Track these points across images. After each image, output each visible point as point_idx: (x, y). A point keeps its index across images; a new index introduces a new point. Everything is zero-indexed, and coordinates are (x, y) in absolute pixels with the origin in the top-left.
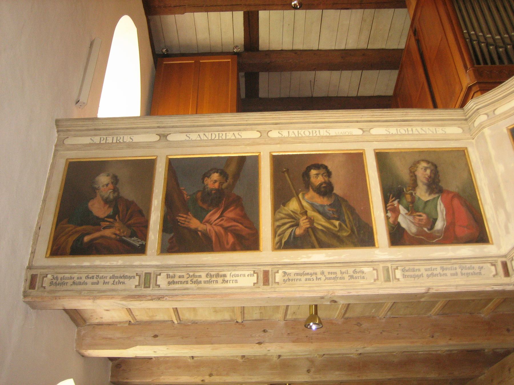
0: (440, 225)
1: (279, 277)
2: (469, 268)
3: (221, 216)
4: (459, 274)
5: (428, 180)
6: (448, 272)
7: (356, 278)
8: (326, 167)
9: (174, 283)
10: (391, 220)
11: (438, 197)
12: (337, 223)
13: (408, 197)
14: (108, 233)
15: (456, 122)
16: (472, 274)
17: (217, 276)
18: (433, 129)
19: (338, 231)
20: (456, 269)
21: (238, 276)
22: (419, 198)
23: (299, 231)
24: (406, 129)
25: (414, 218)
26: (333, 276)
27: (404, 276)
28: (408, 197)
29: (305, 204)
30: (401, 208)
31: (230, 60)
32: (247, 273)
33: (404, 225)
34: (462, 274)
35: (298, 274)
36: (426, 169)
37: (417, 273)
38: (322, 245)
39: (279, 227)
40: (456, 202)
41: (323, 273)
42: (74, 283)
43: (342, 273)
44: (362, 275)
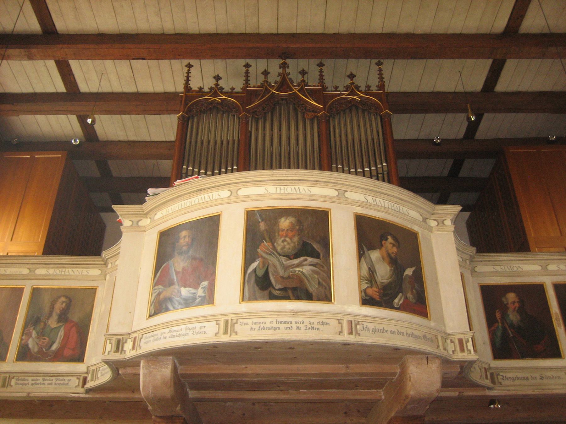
0: (55, 347)
2: (62, 380)
4: (54, 383)
6: (46, 382)
11: (60, 327)
13: (42, 324)
15: (97, 266)
16: (62, 385)
18: (80, 270)
20: (52, 380)
22: (49, 326)
24: (61, 270)
27: (16, 384)
33: (30, 346)
36: (63, 302)
37: (26, 382)
40: (74, 329)
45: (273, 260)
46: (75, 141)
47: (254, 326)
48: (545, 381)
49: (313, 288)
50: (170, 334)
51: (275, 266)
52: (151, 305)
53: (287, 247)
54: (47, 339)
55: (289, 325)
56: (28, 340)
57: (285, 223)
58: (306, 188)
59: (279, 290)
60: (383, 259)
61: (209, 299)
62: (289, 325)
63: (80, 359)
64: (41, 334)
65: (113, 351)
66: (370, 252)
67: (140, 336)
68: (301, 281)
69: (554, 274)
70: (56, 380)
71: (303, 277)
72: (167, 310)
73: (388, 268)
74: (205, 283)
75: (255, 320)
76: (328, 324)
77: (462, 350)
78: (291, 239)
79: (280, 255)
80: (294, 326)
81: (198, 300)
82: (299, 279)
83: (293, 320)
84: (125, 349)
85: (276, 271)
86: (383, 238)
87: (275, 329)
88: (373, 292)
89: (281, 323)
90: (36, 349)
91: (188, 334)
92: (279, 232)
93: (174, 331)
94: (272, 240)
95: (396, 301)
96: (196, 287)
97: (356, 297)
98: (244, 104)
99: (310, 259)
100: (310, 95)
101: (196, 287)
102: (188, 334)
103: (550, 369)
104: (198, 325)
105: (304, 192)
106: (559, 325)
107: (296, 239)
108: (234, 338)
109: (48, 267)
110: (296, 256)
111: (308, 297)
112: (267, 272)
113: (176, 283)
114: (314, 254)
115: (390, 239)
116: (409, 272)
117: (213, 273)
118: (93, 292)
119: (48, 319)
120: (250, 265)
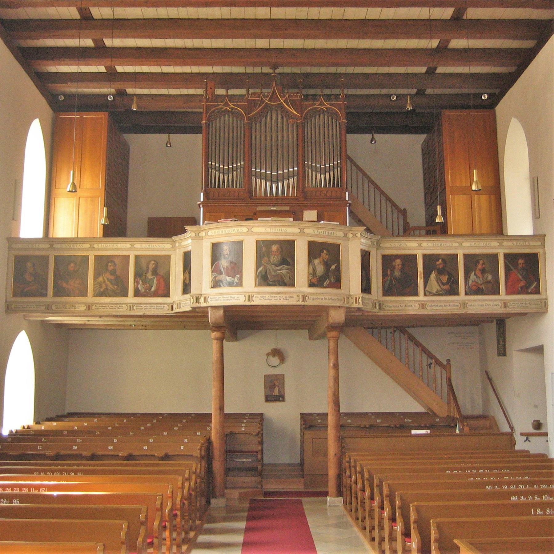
0: (153, 289)
1: (94, 307)
2: (160, 307)
3: (74, 282)
5: (153, 269)
6: (152, 308)
7: (120, 309)
8: (114, 262)
9: (58, 308)
10: (136, 286)
11: (154, 278)
12: (116, 287)
13: (144, 276)
14: (32, 288)
17: (72, 306)
19: (116, 290)
21: (79, 306)
22: (148, 277)
23: (102, 290)
24: (149, 245)
25: (144, 286)
26: (112, 307)
27: (136, 309)
28: (144, 276)
29: (105, 278)
30: (140, 281)
31: (103, 116)
32: (83, 305)
33: (140, 288)
34: (157, 309)
35: (100, 306)
36: (153, 264)
37: (141, 308)
38: (110, 296)
39: (95, 287)
40: (161, 280)
41: (108, 306)
42: (23, 307)
43: (115, 306)
44: (122, 308)
45: (269, 267)
46: (110, 98)
47: (261, 298)
48: (407, 308)
49: (287, 280)
50: (223, 299)
51: (270, 270)
52: (211, 282)
53: (275, 260)
54: (148, 285)
55: (276, 298)
56: (138, 285)
57: (274, 248)
58: (285, 229)
59: (272, 281)
60: (320, 263)
61: (240, 284)
62: (276, 298)
63: (167, 295)
64: (144, 282)
65: (194, 303)
66: (314, 260)
67: (208, 297)
68: (282, 277)
69: (425, 248)
70: (157, 307)
71: (282, 275)
72: (220, 286)
73: (322, 267)
74: (238, 276)
75: (261, 296)
76: (293, 297)
77: (356, 303)
78: (277, 256)
79: (272, 264)
80: (278, 298)
81: (235, 284)
82: (281, 276)
83: (278, 296)
84: (200, 301)
85: (270, 272)
86: (322, 251)
87: (270, 300)
88: (314, 281)
89: (273, 297)
90: (143, 291)
91: (231, 300)
92: (271, 253)
93: (225, 298)
94: (269, 257)
95: (325, 283)
96: (234, 277)
97: (307, 284)
98: (248, 112)
99: (286, 266)
100: (292, 105)
101: (234, 277)
102: (231, 300)
103: (411, 302)
104: (236, 296)
105: (283, 231)
106: (421, 279)
107: (279, 256)
108: (253, 304)
109: (141, 243)
110: (279, 265)
111: (284, 285)
112: (266, 273)
113: (224, 273)
114: (288, 264)
115: (325, 251)
116: (333, 267)
117: (242, 271)
118: (169, 257)
119: (147, 273)
120: (259, 268)
